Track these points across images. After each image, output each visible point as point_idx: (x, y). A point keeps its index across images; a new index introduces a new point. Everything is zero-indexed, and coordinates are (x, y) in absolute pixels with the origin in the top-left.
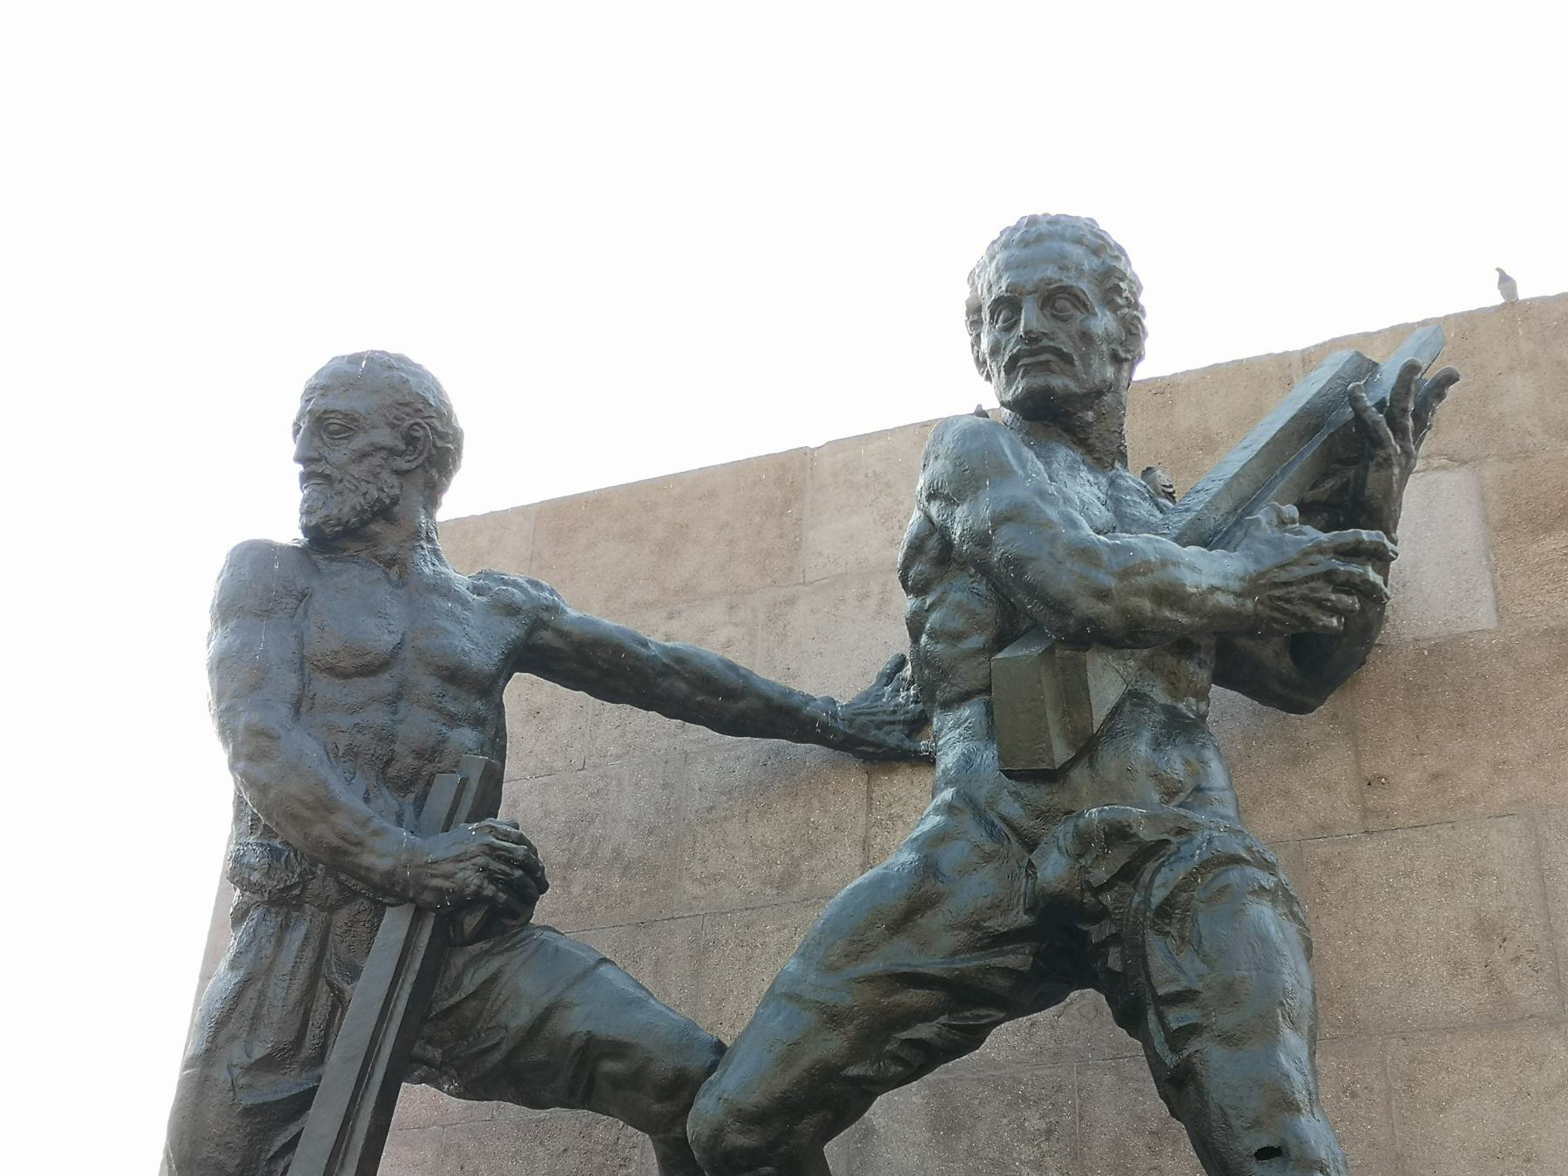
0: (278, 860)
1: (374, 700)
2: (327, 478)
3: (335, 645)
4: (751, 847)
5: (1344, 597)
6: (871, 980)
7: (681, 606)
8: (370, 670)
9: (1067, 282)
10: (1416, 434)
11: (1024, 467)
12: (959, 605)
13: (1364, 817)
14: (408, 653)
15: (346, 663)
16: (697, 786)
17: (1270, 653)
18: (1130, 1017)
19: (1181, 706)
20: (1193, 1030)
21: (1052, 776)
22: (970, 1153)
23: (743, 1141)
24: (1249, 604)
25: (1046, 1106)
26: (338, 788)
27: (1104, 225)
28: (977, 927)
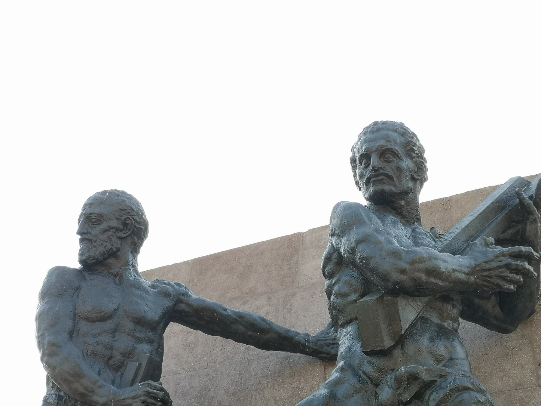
0: (61, 400)
2: (90, 241)
3: (89, 308)
4: (275, 400)
5: (515, 275)
7: (249, 299)
8: (104, 319)
9: (389, 147)
11: (370, 221)
12: (346, 282)
15: (93, 316)
16: (253, 374)
19: (445, 324)
26: (85, 368)
27: (407, 125)
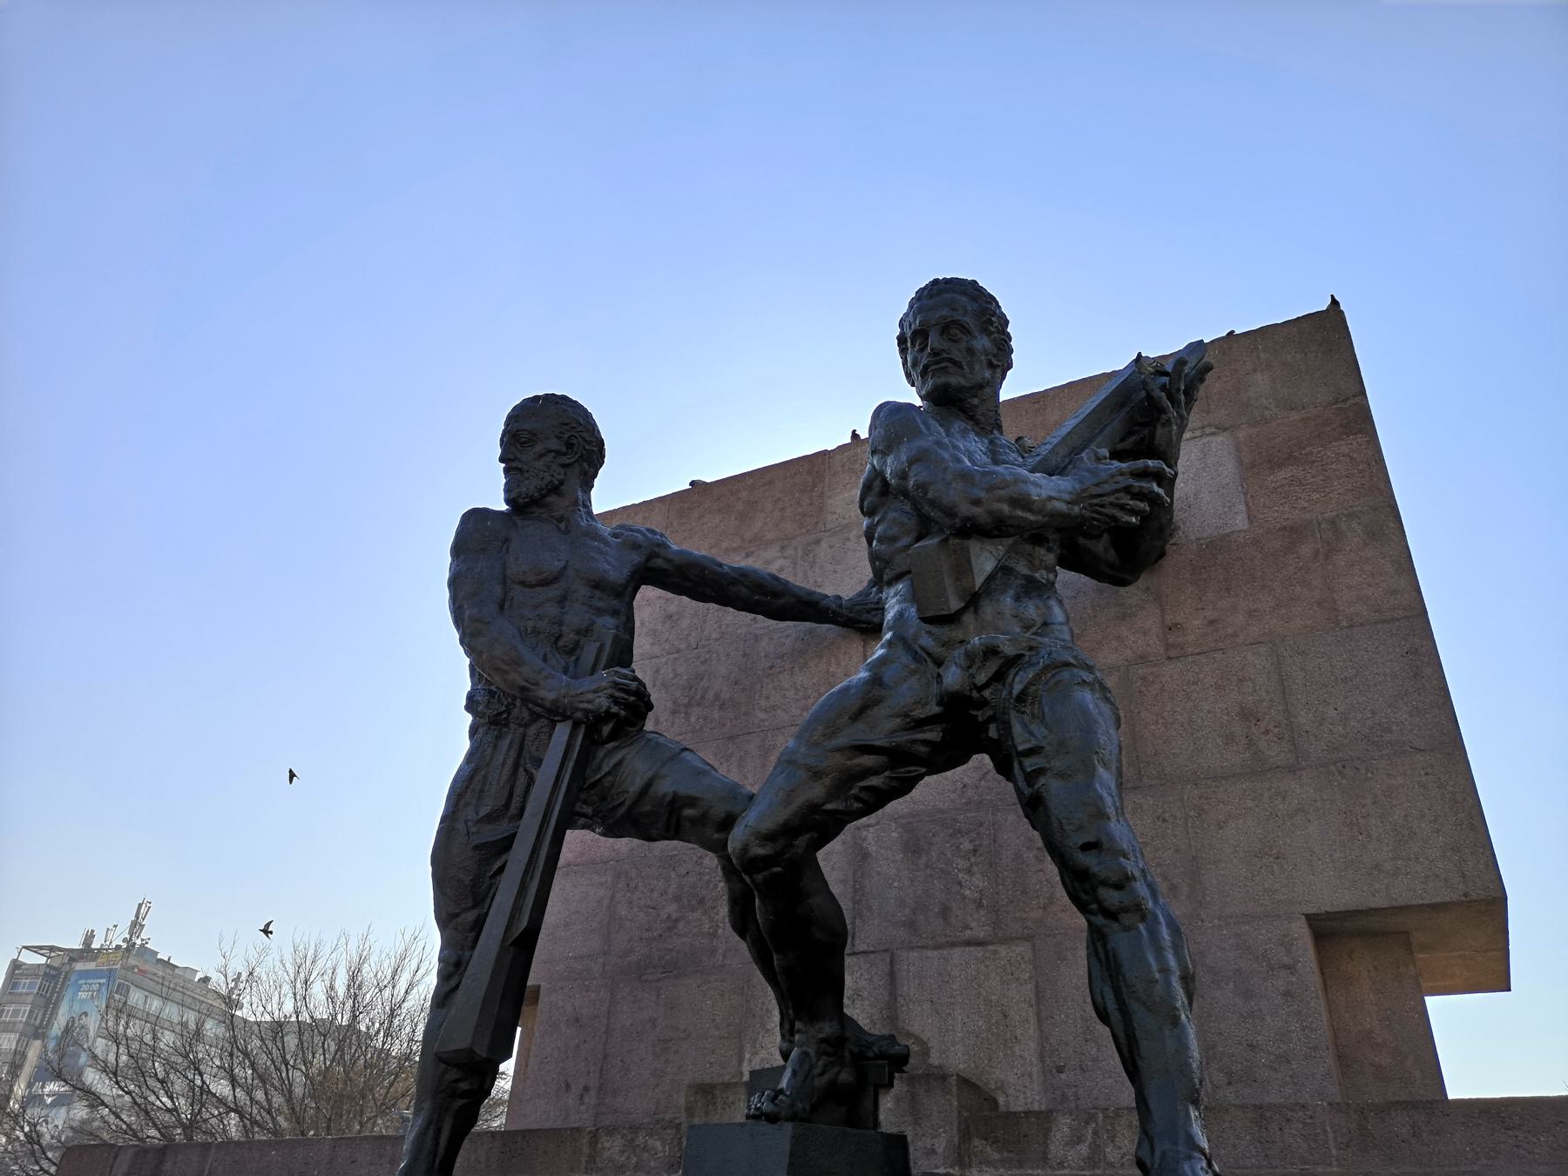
1: (549, 600)
6: (839, 750)
10: (1187, 403)
12: (894, 520)
13: (1167, 650)
14: (570, 572)
15: (532, 579)
17: (1101, 547)
18: (1004, 767)
20: (1041, 772)
21: (951, 619)
23: (761, 851)
25: (974, 835)
28: (907, 716)
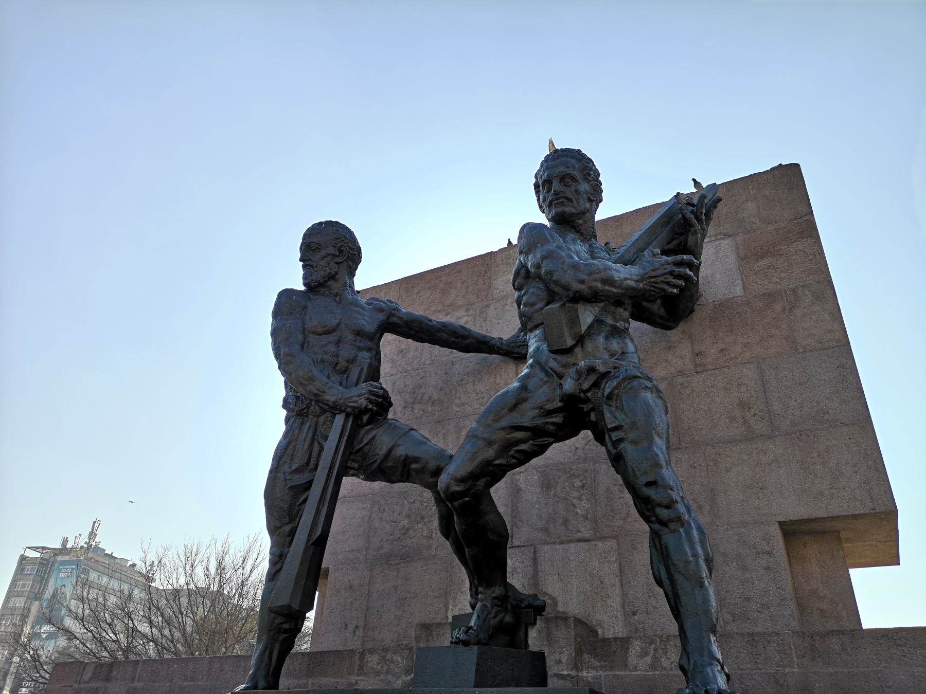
6: (502, 429)
14: (343, 326)
15: (320, 330)
18: (600, 438)
20: (621, 440)
21: (568, 351)
22: (555, 495)
23: (457, 488)
24: (641, 285)
26: (316, 372)
28: (542, 408)
